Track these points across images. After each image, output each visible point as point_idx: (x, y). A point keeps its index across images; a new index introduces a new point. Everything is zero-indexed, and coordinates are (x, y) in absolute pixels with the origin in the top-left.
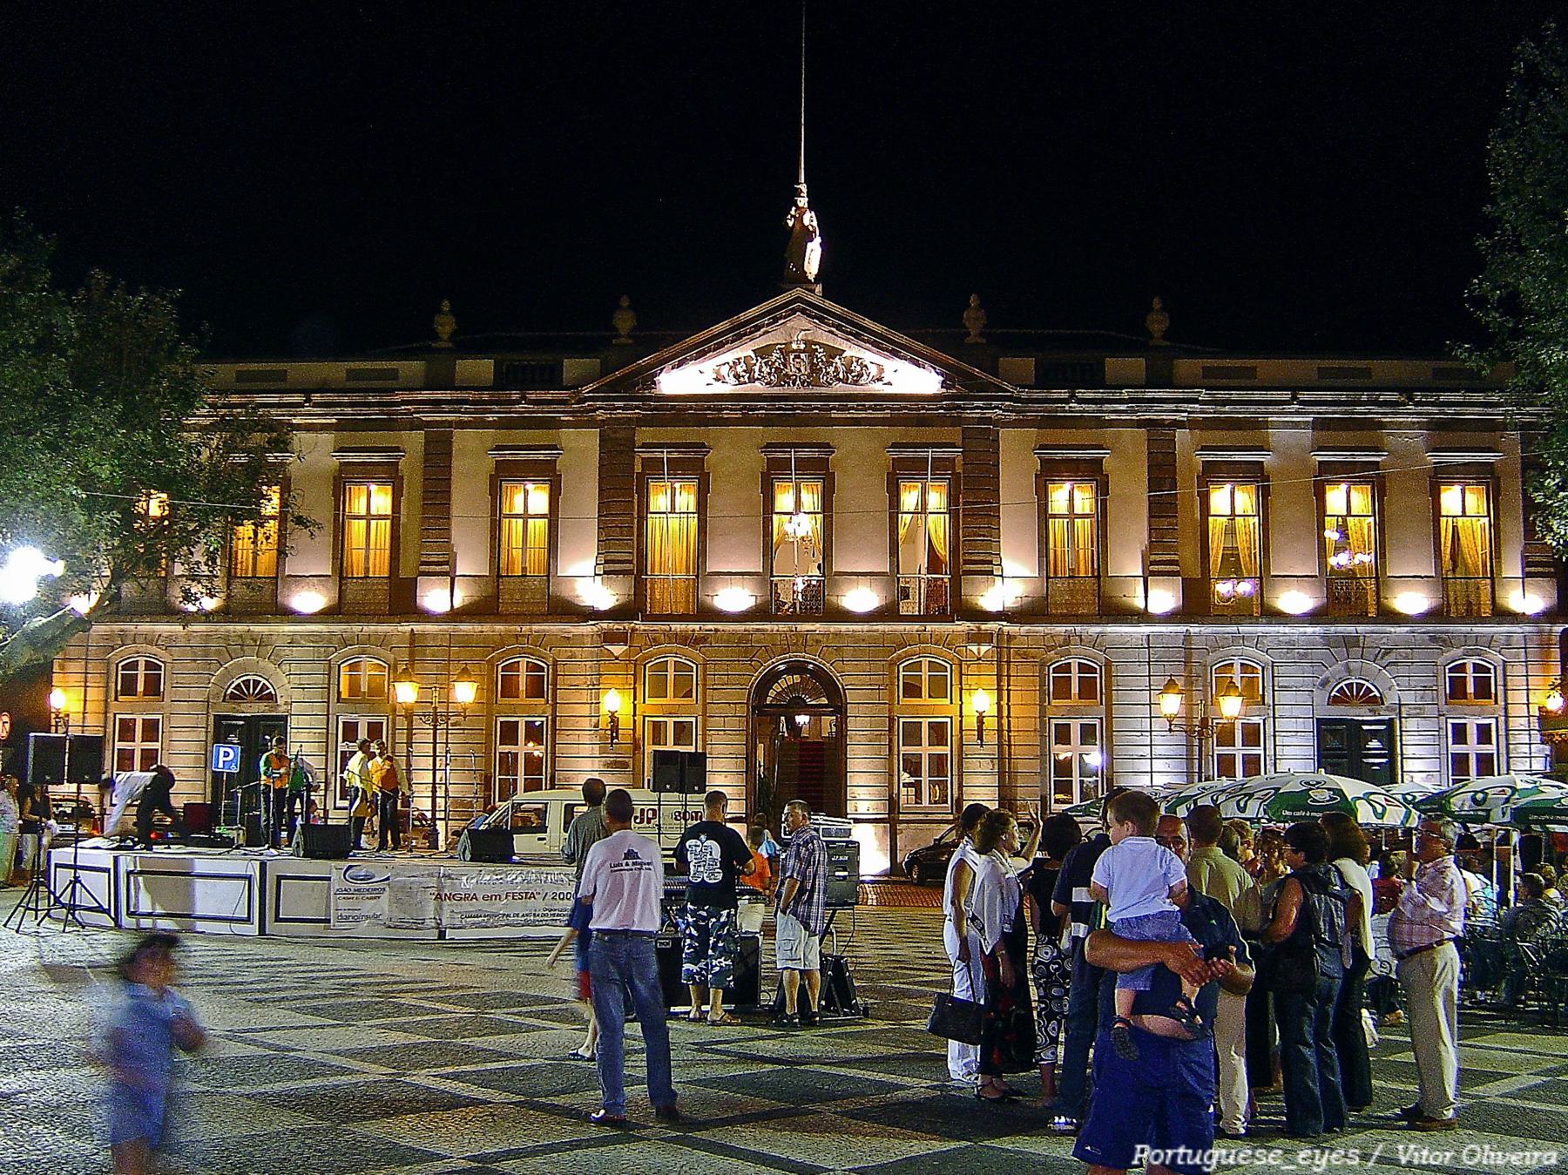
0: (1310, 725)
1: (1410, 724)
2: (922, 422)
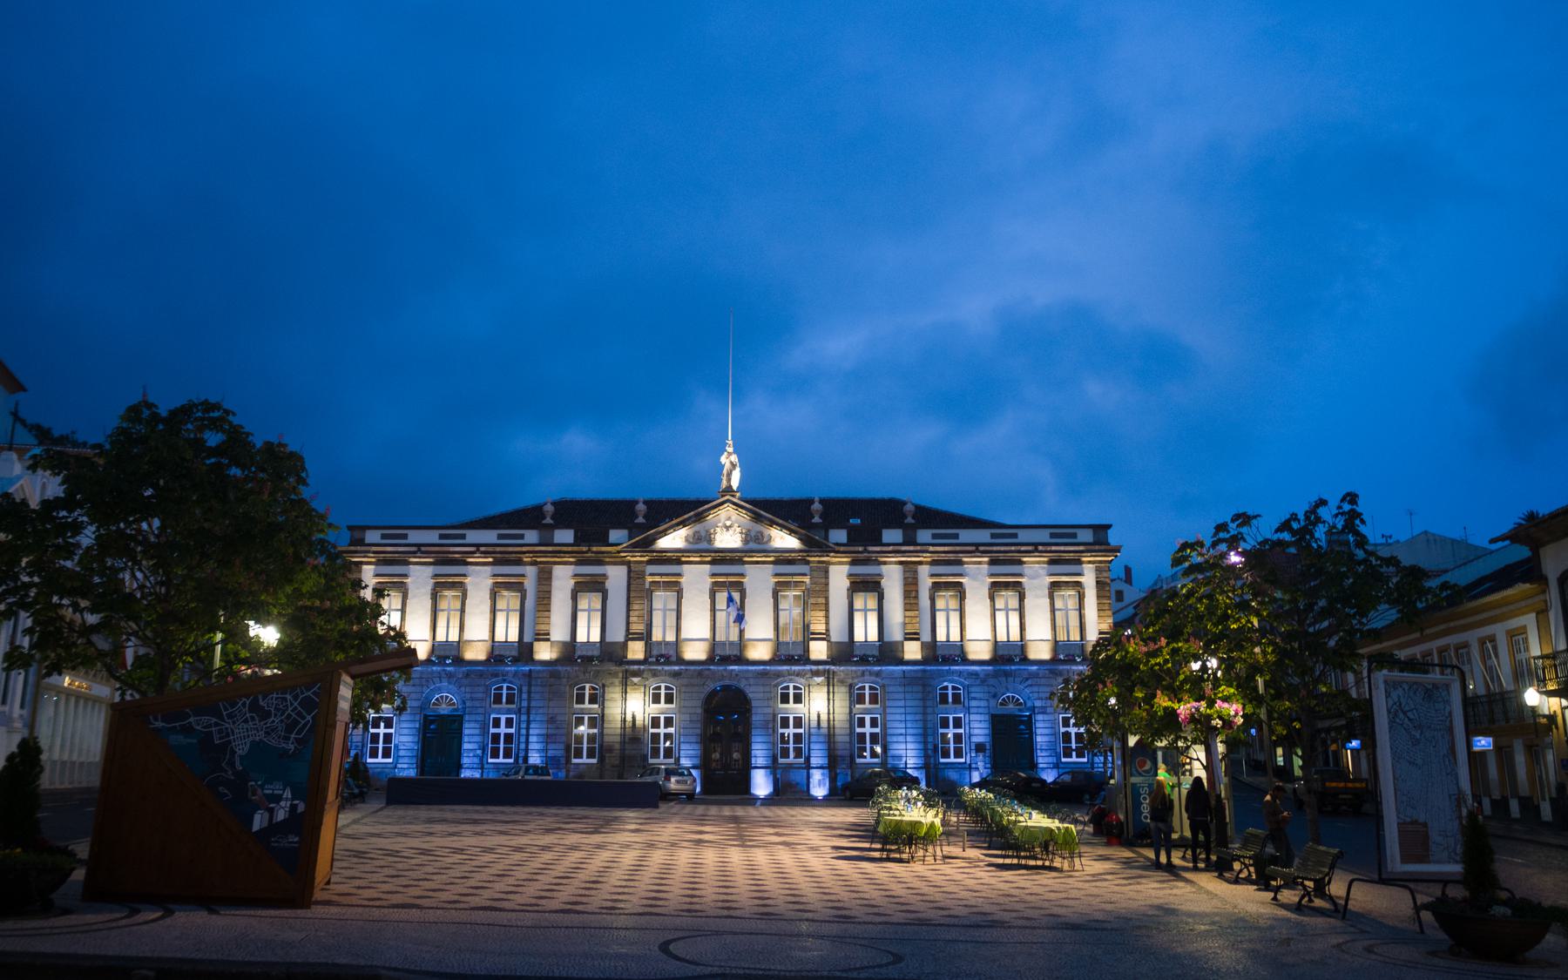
0: (987, 717)
1: (1040, 717)
2: (790, 562)
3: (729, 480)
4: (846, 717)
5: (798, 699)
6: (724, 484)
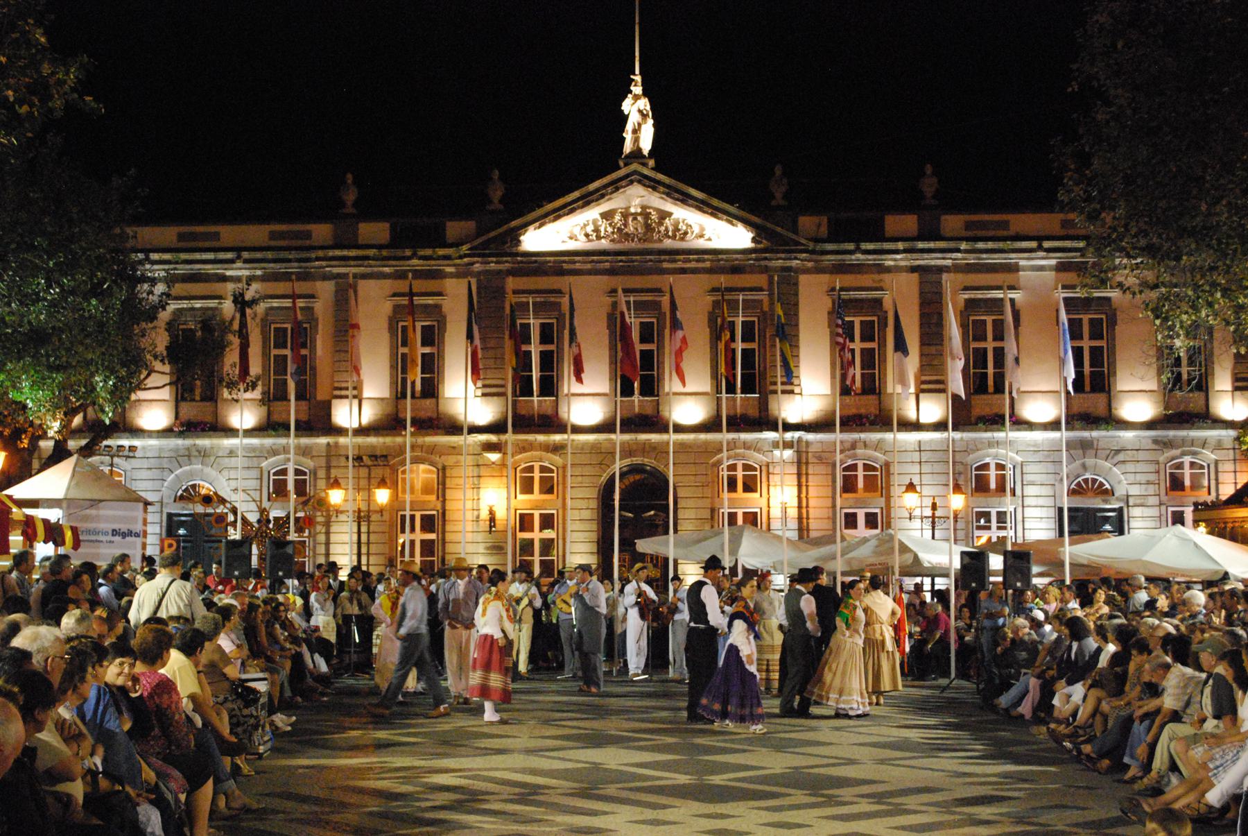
1: (1135, 512)
2: (736, 270)
3: (636, 140)
4: (826, 513)
5: (749, 487)
6: (628, 147)
